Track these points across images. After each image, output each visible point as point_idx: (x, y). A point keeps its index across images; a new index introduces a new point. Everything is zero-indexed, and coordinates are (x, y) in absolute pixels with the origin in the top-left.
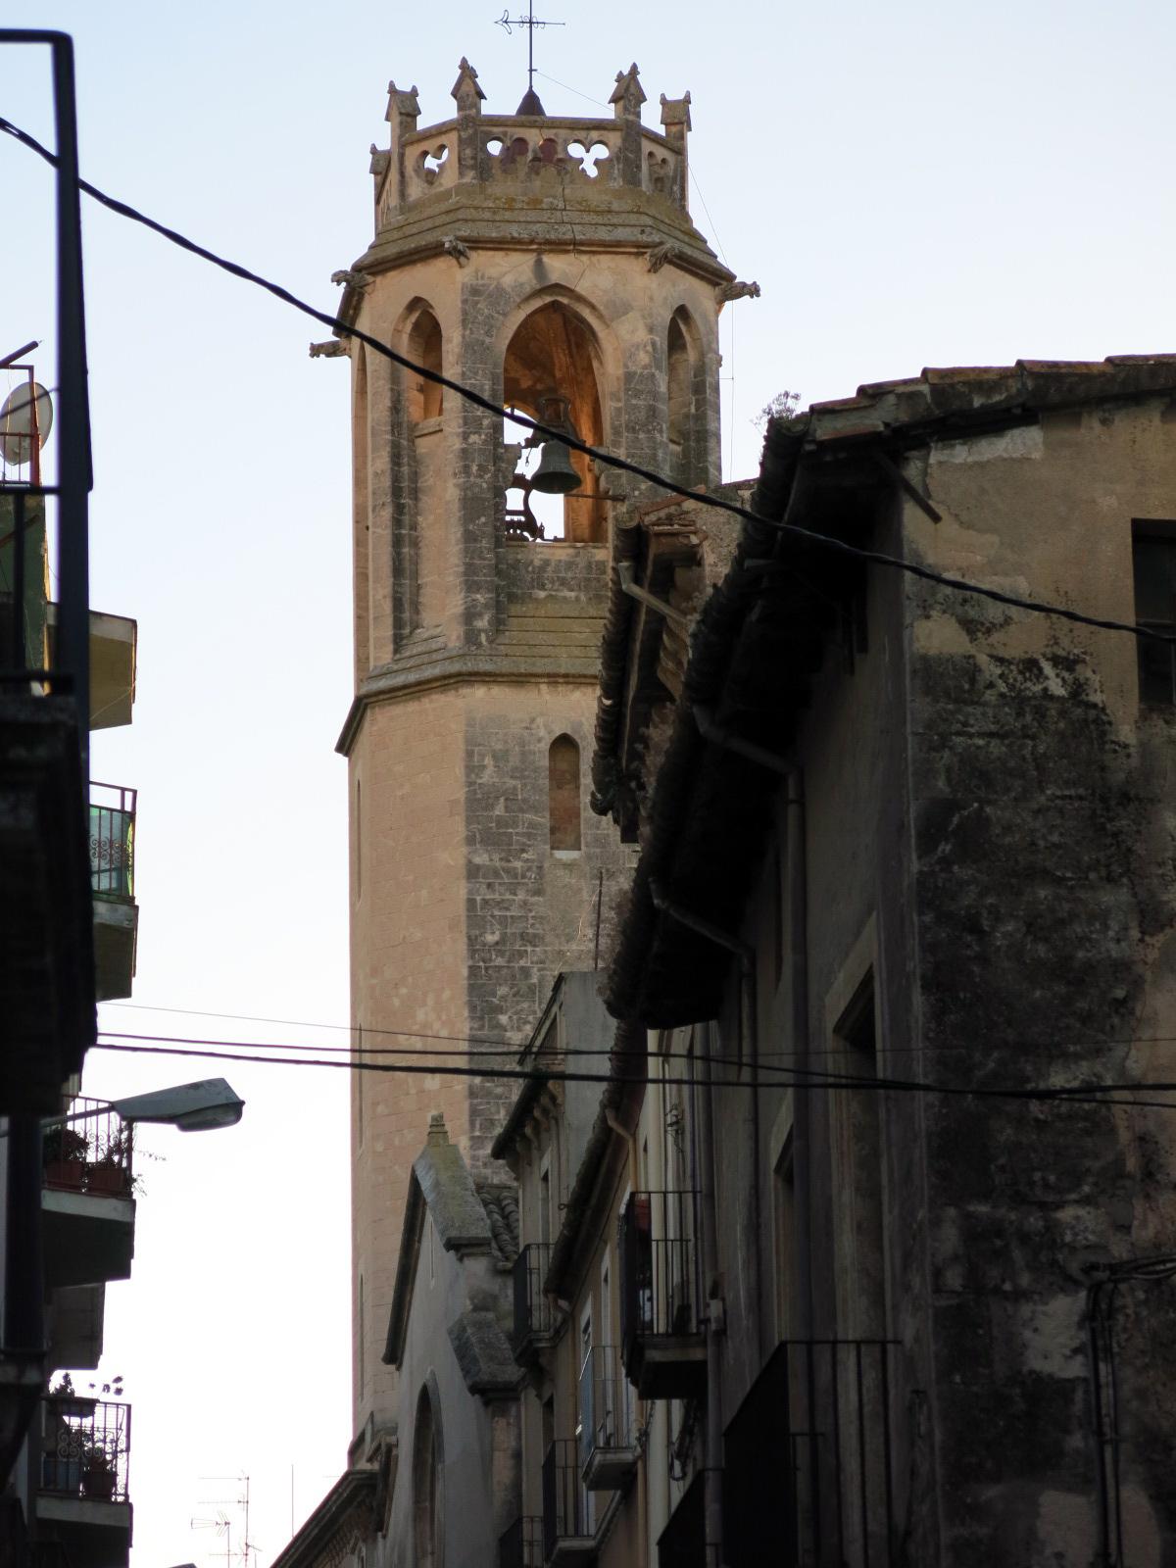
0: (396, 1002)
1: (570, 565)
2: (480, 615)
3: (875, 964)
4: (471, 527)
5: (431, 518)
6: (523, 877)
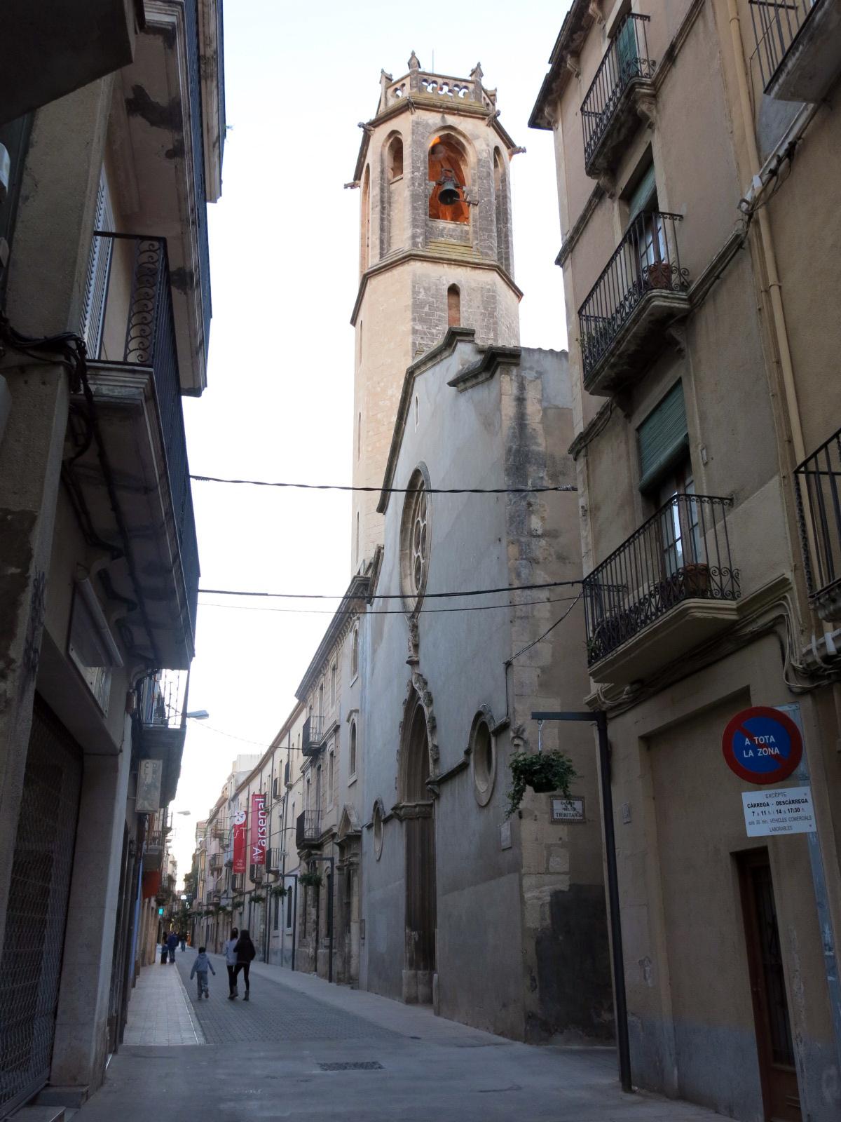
0: (379, 389)
1: (454, 230)
2: (419, 237)
3: (229, 940)
4: (415, 205)
5: (396, 211)
6: (437, 336)
